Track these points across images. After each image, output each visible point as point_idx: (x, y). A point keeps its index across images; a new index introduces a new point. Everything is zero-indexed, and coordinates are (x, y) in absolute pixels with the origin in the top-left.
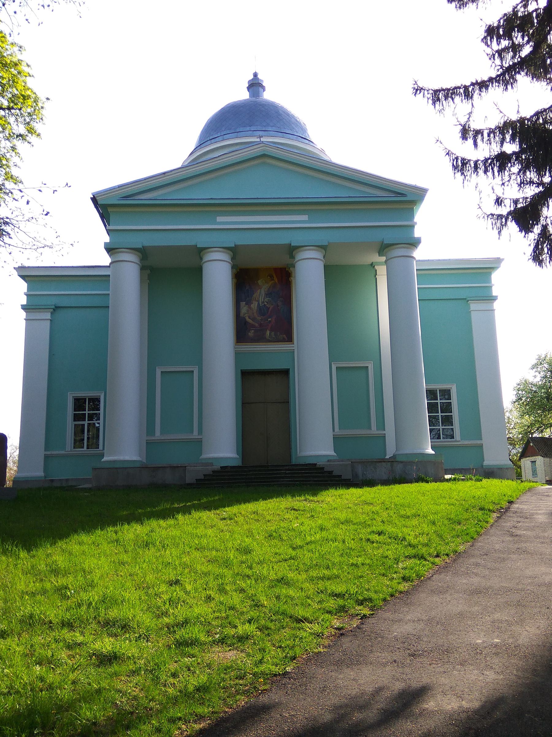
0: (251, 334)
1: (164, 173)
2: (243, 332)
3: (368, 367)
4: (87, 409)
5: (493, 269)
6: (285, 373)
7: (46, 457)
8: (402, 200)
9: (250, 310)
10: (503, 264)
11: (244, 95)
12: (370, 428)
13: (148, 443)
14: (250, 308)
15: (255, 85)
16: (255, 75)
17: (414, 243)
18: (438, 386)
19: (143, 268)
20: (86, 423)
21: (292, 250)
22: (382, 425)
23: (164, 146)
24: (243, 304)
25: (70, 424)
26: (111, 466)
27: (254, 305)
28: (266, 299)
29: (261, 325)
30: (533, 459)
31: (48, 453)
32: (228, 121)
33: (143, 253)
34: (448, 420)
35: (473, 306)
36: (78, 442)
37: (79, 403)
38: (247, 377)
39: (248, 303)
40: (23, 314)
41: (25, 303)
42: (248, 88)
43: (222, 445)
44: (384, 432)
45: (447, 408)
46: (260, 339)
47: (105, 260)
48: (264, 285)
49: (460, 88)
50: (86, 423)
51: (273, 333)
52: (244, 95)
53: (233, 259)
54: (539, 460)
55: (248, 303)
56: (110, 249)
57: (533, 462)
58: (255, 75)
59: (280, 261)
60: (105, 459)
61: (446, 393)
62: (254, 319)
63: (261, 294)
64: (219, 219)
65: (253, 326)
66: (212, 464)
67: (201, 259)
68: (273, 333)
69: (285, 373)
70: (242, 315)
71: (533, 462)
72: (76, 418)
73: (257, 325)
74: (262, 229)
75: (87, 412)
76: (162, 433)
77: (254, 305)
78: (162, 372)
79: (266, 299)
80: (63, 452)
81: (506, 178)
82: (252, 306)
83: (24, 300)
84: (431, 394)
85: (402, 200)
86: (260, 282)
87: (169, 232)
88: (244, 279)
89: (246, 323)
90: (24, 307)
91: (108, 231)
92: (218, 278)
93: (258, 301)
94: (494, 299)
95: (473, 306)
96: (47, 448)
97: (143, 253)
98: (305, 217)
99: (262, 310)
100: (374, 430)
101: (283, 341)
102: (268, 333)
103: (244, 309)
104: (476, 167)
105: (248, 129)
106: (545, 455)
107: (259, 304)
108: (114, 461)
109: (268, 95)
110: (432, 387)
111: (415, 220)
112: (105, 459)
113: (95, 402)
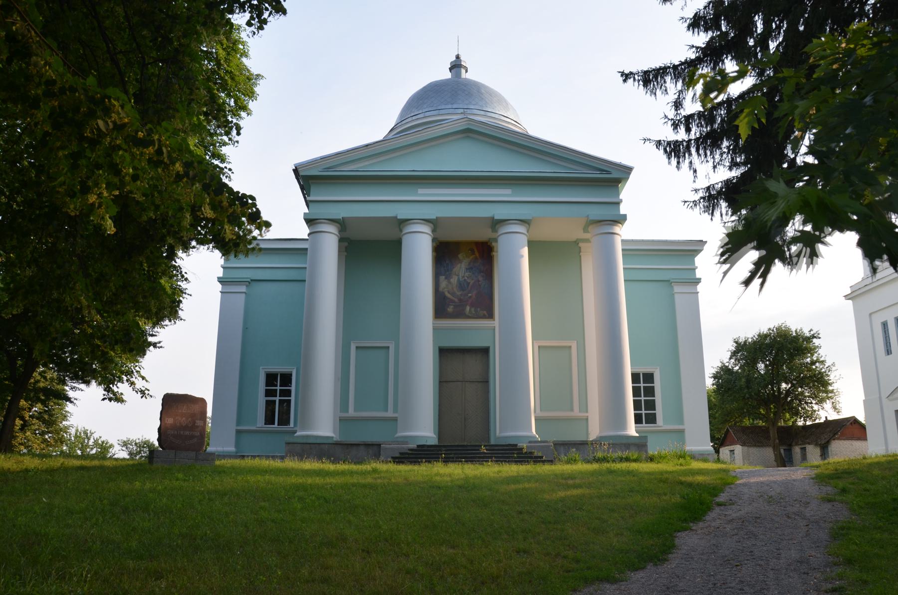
0: (450, 309)
1: (367, 145)
2: (443, 308)
3: (570, 347)
4: (279, 384)
5: (698, 252)
6: (485, 352)
7: (239, 432)
8: (609, 177)
9: (450, 285)
10: (706, 247)
11: (446, 75)
12: (572, 410)
13: (342, 420)
14: (450, 282)
15: (456, 66)
16: (458, 57)
17: (621, 220)
18: (642, 370)
19: (341, 240)
20: (277, 399)
21: (496, 224)
22: (584, 406)
23: (364, 120)
24: (442, 278)
25: (261, 400)
26: (304, 441)
27: (454, 280)
28: (467, 274)
29: (460, 300)
30: (731, 448)
31: (239, 428)
32: (430, 96)
33: (342, 224)
34: (651, 405)
35: (677, 289)
36: (269, 420)
37: (271, 378)
38: (446, 354)
39: (448, 278)
40: (219, 287)
41: (221, 275)
42: (451, 69)
43: (423, 428)
44: (586, 414)
45: (650, 391)
46: (459, 314)
47: (303, 231)
48: (467, 258)
49: (669, 67)
50: (277, 399)
51: (473, 309)
52: (446, 75)
53: (433, 231)
54: (738, 449)
55: (448, 278)
56: (309, 221)
57: (732, 451)
58: (458, 57)
59: (483, 235)
60: (298, 434)
61: (649, 377)
62: (453, 294)
63: (461, 270)
64: (420, 191)
65: (452, 301)
66: (407, 443)
67: (401, 231)
68: (473, 309)
69: (485, 352)
70: (441, 289)
71: (732, 451)
72: (268, 393)
73: (456, 300)
74: (466, 206)
75: (278, 388)
76: (355, 410)
77: (454, 280)
78: (357, 348)
79: (467, 274)
80: (254, 428)
81: (717, 157)
82: (452, 280)
83: (220, 273)
84: (635, 377)
85: (609, 177)
86: (460, 256)
87: (368, 205)
88: (444, 252)
89: (445, 297)
90: (221, 280)
91: (308, 203)
92: (419, 250)
93: (458, 275)
94: (698, 281)
95: (677, 289)
96: (239, 423)
97: (342, 224)
98: (508, 191)
99: (462, 286)
100: (576, 413)
101: (484, 317)
102: (468, 308)
103: (443, 283)
104: (688, 148)
105: (450, 106)
106: (743, 444)
107: (459, 279)
108: (308, 436)
109: (471, 74)
110: (637, 370)
111: (621, 197)
112: (298, 434)
113: (286, 379)
